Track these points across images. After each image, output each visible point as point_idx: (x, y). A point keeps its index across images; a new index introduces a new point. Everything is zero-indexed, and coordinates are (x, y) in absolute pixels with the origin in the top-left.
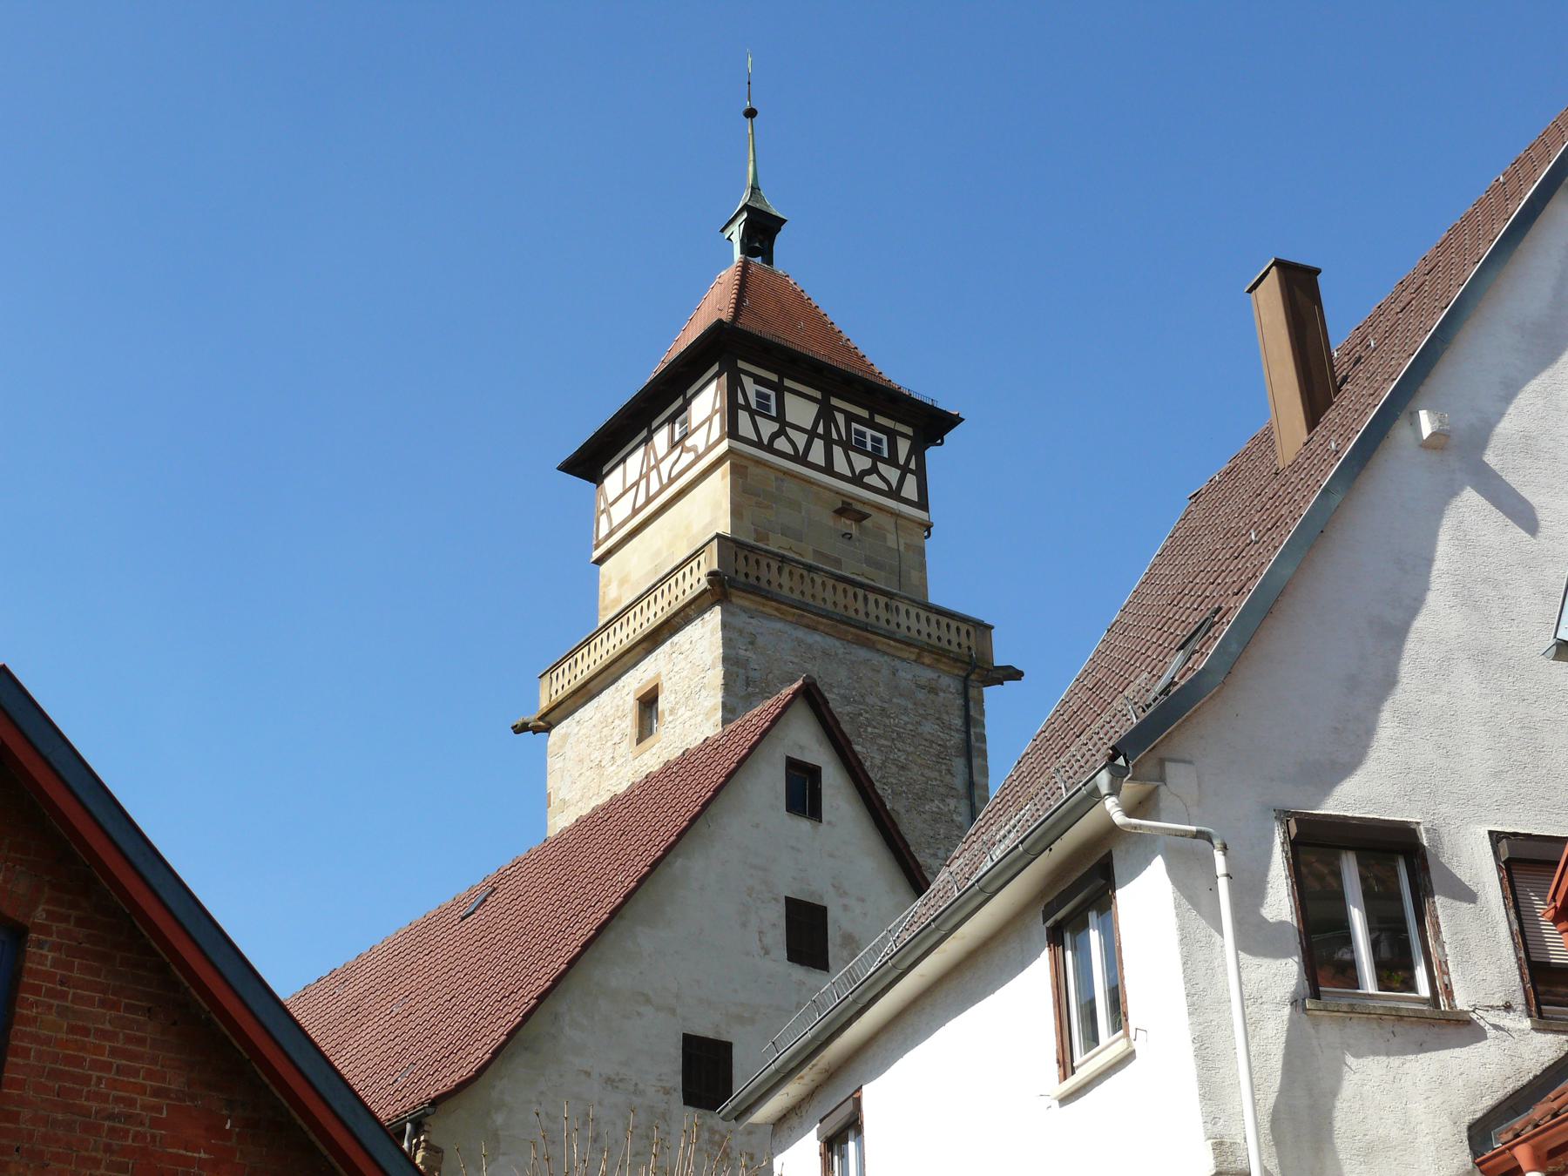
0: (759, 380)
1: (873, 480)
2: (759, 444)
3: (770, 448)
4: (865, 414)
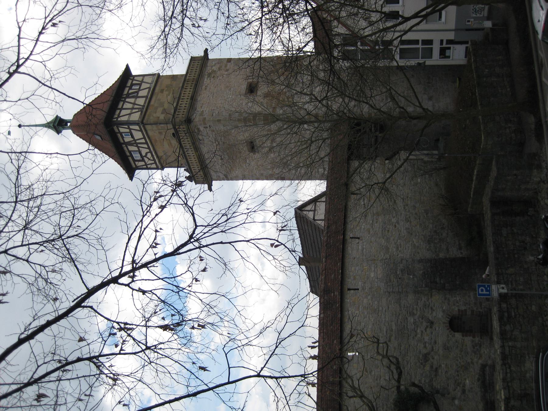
0: (123, 138)
1: (149, 155)
2: (155, 163)
3: (154, 160)
4: (130, 158)
